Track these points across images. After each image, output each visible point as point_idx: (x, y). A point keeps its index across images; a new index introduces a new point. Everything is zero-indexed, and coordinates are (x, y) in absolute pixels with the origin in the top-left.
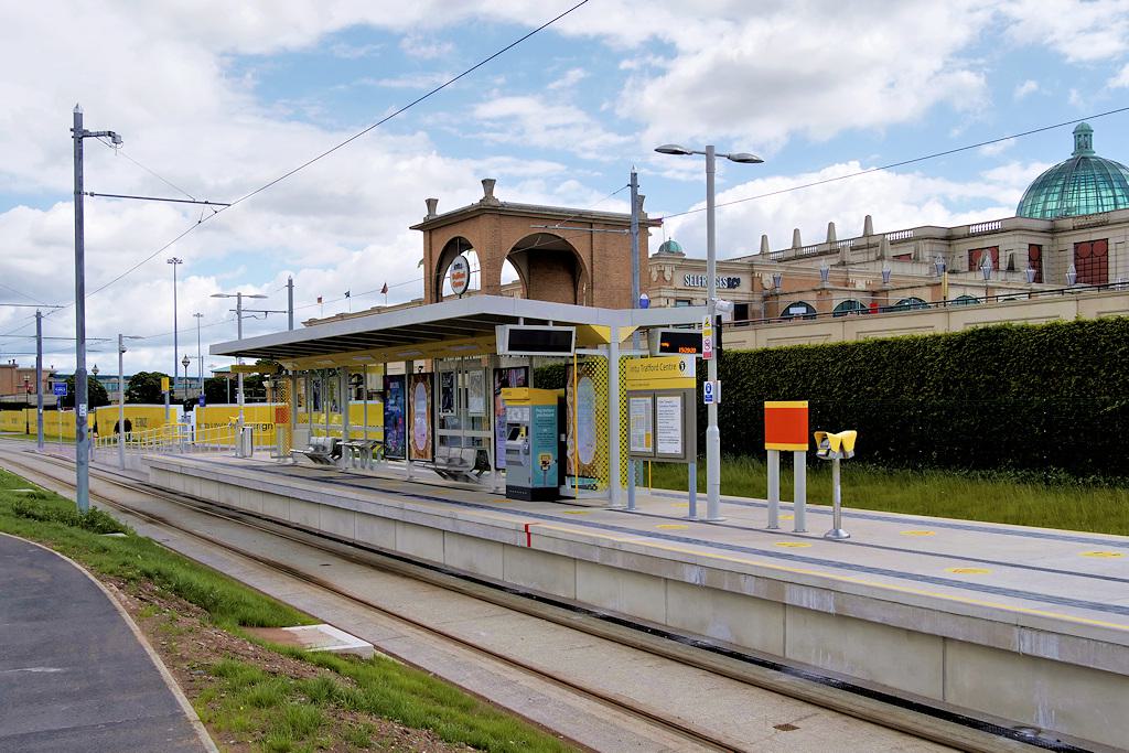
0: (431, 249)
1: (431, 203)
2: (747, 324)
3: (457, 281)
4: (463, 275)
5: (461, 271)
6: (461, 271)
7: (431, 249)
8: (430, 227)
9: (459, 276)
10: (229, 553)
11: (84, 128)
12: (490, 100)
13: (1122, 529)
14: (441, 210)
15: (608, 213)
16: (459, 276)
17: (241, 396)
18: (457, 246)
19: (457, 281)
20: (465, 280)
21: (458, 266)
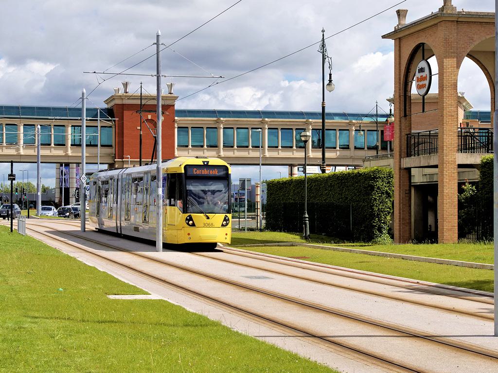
0: (400, 50)
1: (401, 14)
2: (390, 142)
3: (421, 83)
4: (425, 78)
5: (424, 74)
6: (424, 74)
7: (400, 50)
8: (398, 36)
9: (422, 79)
10: (250, 265)
11: (386, 108)
12: (425, 243)
13: (1, 107)
14: (409, 20)
15: (342, 247)
16: (422, 79)
17: (40, 206)
18: (421, 52)
19: (421, 83)
20: (427, 82)
21: (422, 70)
